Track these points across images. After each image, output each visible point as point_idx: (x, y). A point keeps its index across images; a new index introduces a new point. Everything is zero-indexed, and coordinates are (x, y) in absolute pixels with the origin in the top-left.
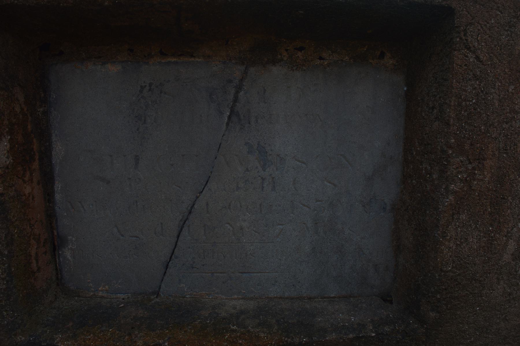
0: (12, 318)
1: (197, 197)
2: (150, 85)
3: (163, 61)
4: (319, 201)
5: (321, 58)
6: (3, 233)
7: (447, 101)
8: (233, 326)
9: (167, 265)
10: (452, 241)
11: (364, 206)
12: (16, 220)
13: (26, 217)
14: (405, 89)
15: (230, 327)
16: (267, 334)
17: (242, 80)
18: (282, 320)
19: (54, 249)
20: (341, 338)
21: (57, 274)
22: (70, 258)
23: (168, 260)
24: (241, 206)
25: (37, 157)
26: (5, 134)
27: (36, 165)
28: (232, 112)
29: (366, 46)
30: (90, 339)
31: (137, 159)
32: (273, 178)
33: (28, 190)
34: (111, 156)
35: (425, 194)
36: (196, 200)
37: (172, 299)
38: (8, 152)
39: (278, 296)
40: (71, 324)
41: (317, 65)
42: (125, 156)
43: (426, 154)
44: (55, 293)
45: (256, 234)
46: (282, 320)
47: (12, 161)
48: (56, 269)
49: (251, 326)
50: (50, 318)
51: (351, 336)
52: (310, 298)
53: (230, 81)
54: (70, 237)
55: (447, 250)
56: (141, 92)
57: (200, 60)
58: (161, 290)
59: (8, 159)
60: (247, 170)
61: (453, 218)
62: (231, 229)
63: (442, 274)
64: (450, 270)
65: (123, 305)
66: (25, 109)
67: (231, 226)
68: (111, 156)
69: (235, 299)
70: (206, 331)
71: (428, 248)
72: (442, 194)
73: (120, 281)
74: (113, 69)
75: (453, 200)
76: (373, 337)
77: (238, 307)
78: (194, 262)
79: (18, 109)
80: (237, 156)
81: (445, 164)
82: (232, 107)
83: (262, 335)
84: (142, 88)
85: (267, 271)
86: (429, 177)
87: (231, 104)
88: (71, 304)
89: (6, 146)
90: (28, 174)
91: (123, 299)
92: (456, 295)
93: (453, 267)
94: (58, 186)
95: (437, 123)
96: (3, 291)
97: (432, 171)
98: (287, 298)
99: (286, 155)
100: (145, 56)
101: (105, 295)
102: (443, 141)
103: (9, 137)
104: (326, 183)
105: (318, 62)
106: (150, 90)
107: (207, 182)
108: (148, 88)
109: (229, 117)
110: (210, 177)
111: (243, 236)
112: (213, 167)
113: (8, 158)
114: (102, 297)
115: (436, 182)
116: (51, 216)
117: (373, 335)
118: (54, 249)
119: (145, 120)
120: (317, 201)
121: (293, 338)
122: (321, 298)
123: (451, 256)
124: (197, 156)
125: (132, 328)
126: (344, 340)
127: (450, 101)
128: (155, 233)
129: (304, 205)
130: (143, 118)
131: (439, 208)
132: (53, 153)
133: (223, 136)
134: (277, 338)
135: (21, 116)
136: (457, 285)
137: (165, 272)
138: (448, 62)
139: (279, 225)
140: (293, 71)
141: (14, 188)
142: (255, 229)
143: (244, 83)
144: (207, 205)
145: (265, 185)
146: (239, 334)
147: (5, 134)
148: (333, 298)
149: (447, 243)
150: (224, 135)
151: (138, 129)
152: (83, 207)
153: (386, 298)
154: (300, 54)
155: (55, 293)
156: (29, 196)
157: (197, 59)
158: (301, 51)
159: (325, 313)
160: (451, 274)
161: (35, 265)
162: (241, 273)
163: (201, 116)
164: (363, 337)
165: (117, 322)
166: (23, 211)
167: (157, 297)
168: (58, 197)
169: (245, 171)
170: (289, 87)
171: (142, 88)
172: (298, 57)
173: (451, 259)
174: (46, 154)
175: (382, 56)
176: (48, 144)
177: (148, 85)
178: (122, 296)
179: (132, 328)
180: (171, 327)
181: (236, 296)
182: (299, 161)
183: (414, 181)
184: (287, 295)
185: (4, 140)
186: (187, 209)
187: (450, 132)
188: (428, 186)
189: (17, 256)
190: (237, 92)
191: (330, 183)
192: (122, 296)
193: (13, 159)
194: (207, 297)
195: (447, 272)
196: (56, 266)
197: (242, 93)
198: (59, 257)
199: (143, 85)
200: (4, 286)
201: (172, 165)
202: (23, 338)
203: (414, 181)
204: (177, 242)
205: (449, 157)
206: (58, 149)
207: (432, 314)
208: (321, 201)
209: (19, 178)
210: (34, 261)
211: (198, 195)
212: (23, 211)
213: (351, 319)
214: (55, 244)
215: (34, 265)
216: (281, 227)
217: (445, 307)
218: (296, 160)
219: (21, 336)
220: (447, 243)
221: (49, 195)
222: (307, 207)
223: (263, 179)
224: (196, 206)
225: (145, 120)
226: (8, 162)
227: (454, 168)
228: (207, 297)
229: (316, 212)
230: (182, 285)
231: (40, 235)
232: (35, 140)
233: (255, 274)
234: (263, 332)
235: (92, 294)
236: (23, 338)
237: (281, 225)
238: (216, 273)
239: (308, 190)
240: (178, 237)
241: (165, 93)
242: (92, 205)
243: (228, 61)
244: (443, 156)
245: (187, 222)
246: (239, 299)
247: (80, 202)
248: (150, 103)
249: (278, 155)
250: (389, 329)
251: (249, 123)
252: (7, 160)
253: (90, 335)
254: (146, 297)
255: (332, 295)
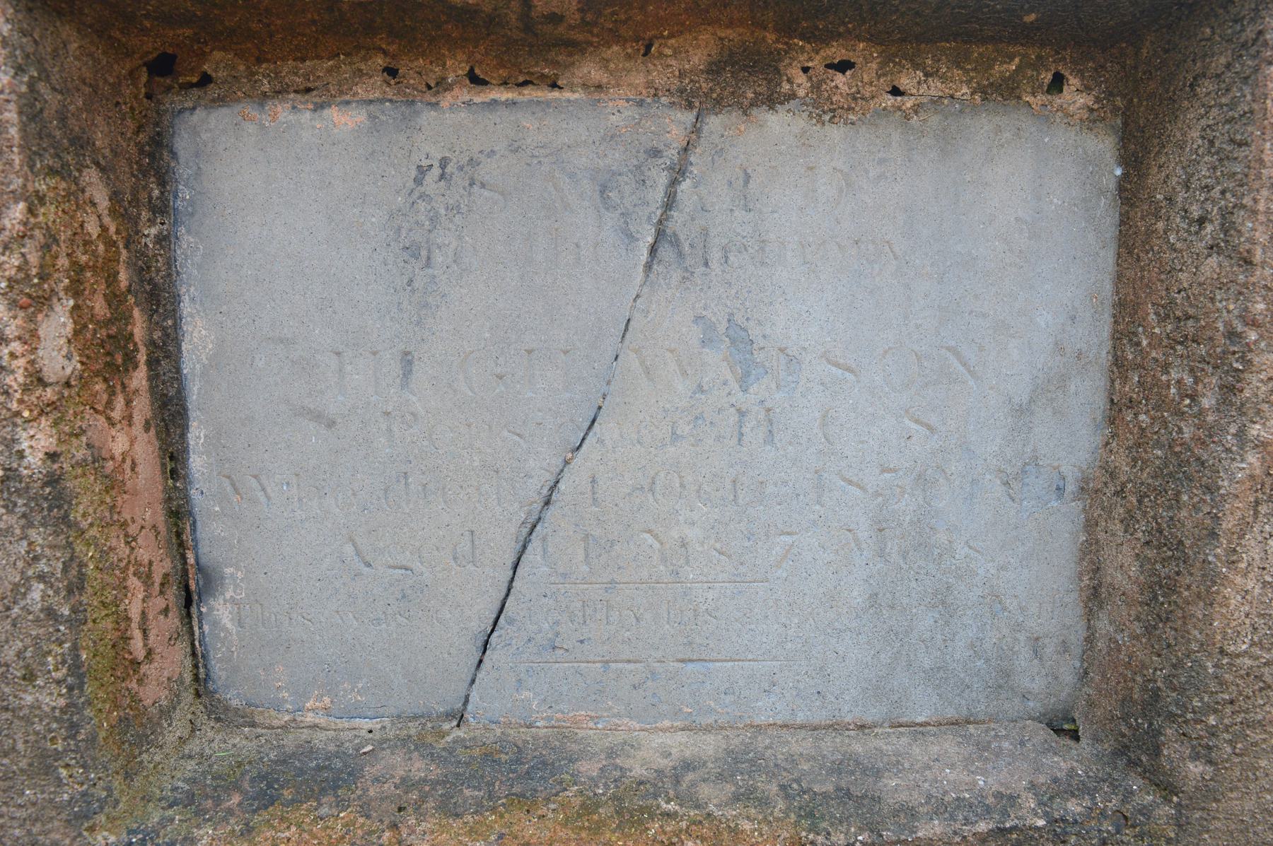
0: (82, 784)
1: (567, 462)
2: (444, 163)
3: (477, 100)
4: (889, 470)
5: (896, 92)
6: (58, 559)
7: (1247, 201)
8: (668, 802)
9: (487, 642)
10: (1251, 575)
11: (1007, 483)
12: (91, 525)
13: (116, 517)
14: (1118, 172)
15: (658, 807)
16: (759, 823)
17: (686, 150)
18: (795, 786)
19: (188, 602)
20: (955, 833)
21: (196, 666)
22: (229, 625)
23: (489, 629)
24: (682, 486)
25: (142, 357)
26: (62, 294)
27: (139, 378)
28: (660, 234)
29: (1017, 60)
30: (289, 840)
31: (407, 361)
32: (769, 410)
33: (119, 445)
34: (338, 354)
35: (1177, 449)
36: (562, 471)
37: (498, 732)
38: (69, 341)
39: (779, 722)
40: (236, 799)
41: (885, 109)
42: (374, 353)
43: (1181, 343)
44: (189, 716)
45: (722, 557)
46: (795, 786)
47: (79, 366)
48: (194, 654)
49: (715, 801)
50: (180, 784)
51: (982, 827)
52: (862, 727)
53: (655, 153)
54: (228, 571)
55: (1239, 598)
56: (418, 181)
57: (576, 96)
58: (470, 707)
59: (70, 360)
60: (700, 389)
61: (1256, 513)
62: (657, 545)
63: (1224, 662)
64: (1245, 652)
65: (369, 748)
66: (112, 229)
67: (656, 537)
68: (338, 354)
69: (664, 730)
70: (596, 817)
71: (1186, 593)
72: (1228, 450)
73: (360, 685)
74: (344, 120)
75: (1257, 464)
76: (1038, 829)
77: (674, 751)
78: (557, 634)
79: (93, 229)
80: (672, 351)
81: (1237, 370)
82: (660, 222)
83: (747, 826)
84: (422, 171)
85: (750, 657)
86: (1189, 406)
87: (659, 212)
88: (234, 746)
89: (64, 325)
90: (120, 402)
91: (370, 732)
92: (1259, 717)
93: (1253, 644)
94: (197, 434)
95: (1213, 261)
96: (57, 713)
97: (1200, 387)
98: (802, 727)
99: (804, 349)
100: (429, 87)
101: (322, 720)
102: (1231, 307)
103: (71, 303)
104: (907, 421)
105: (890, 100)
106: (442, 177)
107: (594, 421)
108: (436, 171)
109: (653, 250)
110: (600, 408)
111: (687, 562)
112: (608, 383)
113: (68, 357)
114: (314, 727)
115: (1210, 418)
116: (178, 514)
117: (1041, 823)
118: (188, 602)
119: (429, 258)
120: (883, 471)
121: (829, 834)
122: (891, 727)
123: (1247, 615)
124: (566, 352)
125: (400, 809)
126: (965, 837)
127: (1255, 201)
128: (455, 558)
129: (850, 482)
130: (424, 253)
131: (1219, 488)
132: (184, 347)
133: (635, 300)
134: (786, 834)
135: (101, 248)
136: (1261, 689)
137: (481, 661)
138: (1249, 97)
139: (783, 533)
140: (823, 124)
141: (84, 439)
142: (718, 546)
143: (692, 159)
144: (594, 481)
145: (745, 430)
146: (684, 824)
147: (62, 294)
148: (921, 725)
149: (1239, 580)
150: (638, 296)
151: (410, 282)
152: (264, 489)
153: (1063, 727)
154: (840, 79)
155: (189, 716)
156: (124, 460)
157: (567, 95)
158: (844, 72)
159: (907, 765)
160: (1248, 662)
161: (140, 644)
162: (682, 661)
163: (577, 246)
164: (1014, 828)
165: (359, 792)
166: (108, 500)
167: (458, 726)
168: (197, 463)
169: (695, 393)
170: (811, 169)
171: (422, 171)
172: (837, 87)
173: (1247, 621)
174: (165, 351)
175: (1058, 83)
176: (170, 322)
177: (436, 164)
178: (366, 724)
179: (400, 809)
180: (503, 805)
181: (667, 723)
182: (837, 365)
183: (1142, 417)
184: (800, 718)
185: (58, 308)
186: (539, 493)
187: (1254, 284)
188: (1185, 430)
189: (94, 621)
190: (674, 183)
191: (917, 421)
192: (366, 724)
193: (82, 363)
194: (591, 725)
195: (1238, 656)
196: (193, 645)
197: (685, 185)
198: (200, 622)
199: (425, 163)
200: (62, 702)
201: (500, 377)
202: (112, 839)
203: (1142, 417)
204: (512, 579)
205: (1250, 351)
206: (198, 339)
207: (1195, 769)
208: (894, 471)
209: (96, 411)
210: (137, 634)
211: (570, 455)
212: (108, 500)
213: (975, 783)
214: (190, 592)
215: (137, 646)
216: (788, 539)
217: (1229, 750)
218: (829, 361)
219: (106, 833)
220: (1239, 580)
221: (174, 461)
222: (858, 486)
223: (742, 413)
224: (562, 486)
225: (429, 258)
226: (68, 371)
227: (1262, 381)
228: (591, 725)
229: (880, 499)
230: (526, 694)
231: (151, 563)
232: (136, 313)
233: (718, 664)
234: (748, 818)
235: (287, 718)
236: (112, 839)
237: (788, 534)
238: (616, 661)
239: (862, 442)
240: (515, 567)
241: (483, 186)
242: (288, 484)
243: (649, 100)
244: (1232, 348)
245: (538, 528)
246: (676, 730)
247: (255, 477)
248: (443, 212)
249: (782, 350)
250: (1079, 809)
251: (706, 264)
252: (67, 362)
253: (288, 828)
254: (429, 725)
255: (920, 719)
